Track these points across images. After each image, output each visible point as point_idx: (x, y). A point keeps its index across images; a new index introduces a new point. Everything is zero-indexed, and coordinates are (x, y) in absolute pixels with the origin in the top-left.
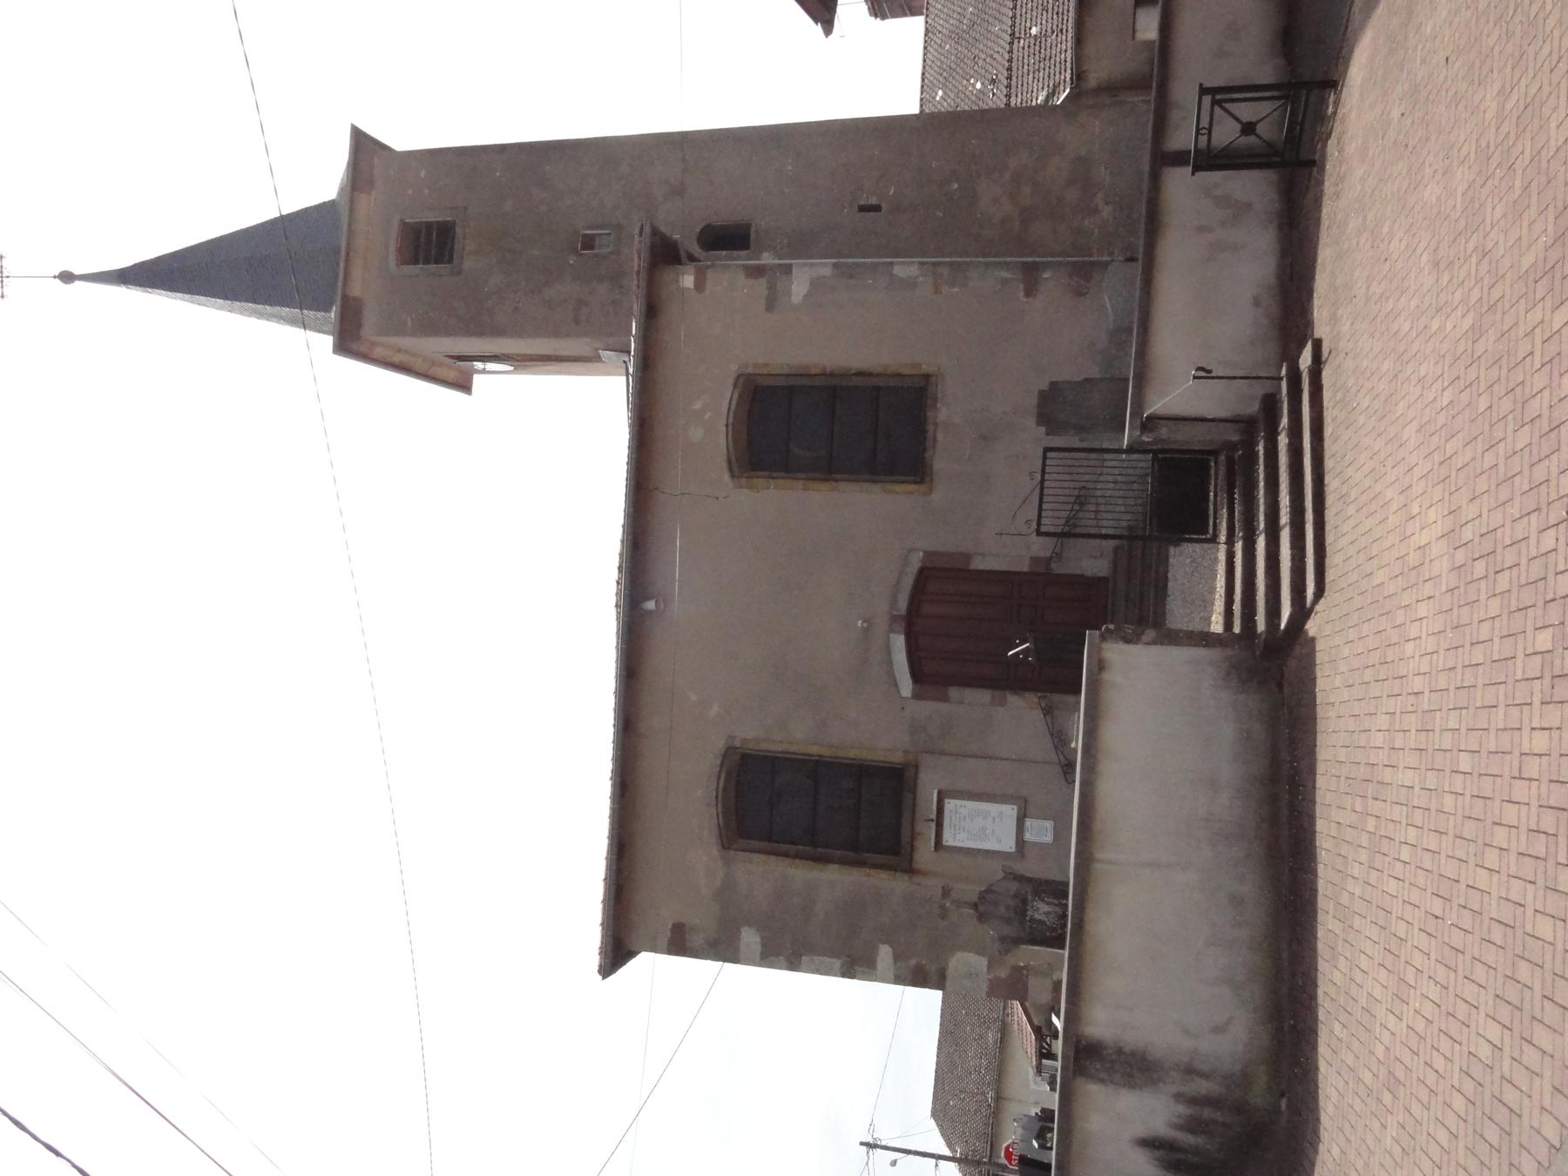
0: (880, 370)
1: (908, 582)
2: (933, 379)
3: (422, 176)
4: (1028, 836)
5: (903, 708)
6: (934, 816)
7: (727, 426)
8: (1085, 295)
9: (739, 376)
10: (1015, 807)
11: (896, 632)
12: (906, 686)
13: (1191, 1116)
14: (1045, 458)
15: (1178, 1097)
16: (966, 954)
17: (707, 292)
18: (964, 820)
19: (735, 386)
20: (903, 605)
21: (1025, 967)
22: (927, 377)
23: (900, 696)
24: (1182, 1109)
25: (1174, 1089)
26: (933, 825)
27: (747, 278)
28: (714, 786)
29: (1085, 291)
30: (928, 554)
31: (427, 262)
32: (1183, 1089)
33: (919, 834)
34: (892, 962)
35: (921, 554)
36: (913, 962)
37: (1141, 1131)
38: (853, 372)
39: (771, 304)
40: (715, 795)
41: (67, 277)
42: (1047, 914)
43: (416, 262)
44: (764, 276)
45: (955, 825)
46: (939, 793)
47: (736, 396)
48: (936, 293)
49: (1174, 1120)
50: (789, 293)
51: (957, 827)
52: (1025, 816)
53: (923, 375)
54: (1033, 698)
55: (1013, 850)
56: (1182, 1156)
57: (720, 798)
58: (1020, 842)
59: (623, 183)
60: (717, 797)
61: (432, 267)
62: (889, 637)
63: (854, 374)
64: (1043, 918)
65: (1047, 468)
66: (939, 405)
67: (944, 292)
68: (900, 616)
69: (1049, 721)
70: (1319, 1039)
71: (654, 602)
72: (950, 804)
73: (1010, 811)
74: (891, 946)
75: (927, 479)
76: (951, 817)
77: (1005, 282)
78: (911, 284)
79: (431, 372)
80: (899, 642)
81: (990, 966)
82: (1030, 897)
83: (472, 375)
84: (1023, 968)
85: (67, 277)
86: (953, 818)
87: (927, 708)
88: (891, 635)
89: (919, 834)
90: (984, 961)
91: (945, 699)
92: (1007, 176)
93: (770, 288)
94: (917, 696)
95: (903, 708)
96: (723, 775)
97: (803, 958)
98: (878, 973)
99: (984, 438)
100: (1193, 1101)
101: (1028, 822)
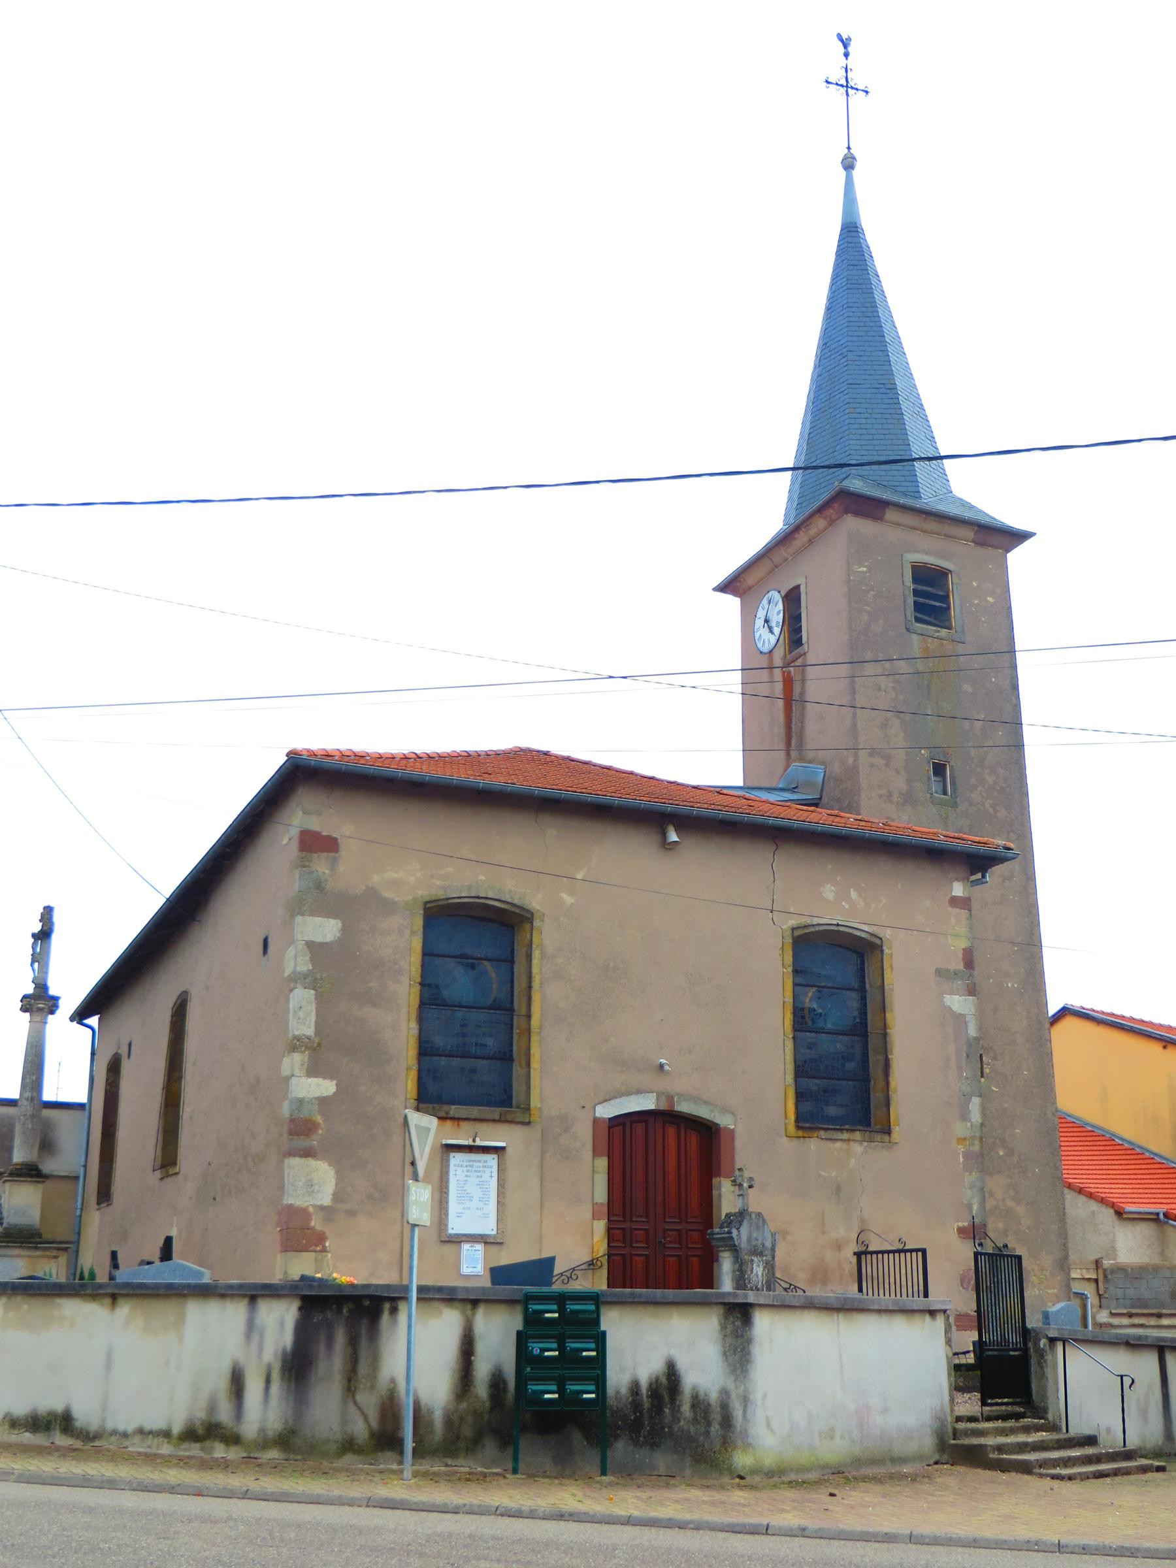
0: (893, 1084)
1: (704, 1112)
2: (886, 1138)
3: (988, 599)
4: (466, 1247)
5: (583, 1107)
6: (479, 1142)
7: (838, 925)
8: (962, 1284)
9: (881, 939)
10: (494, 1232)
11: (658, 1099)
12: (607, 1111)
13: (709, 1404)
14: (917, 1250)
15: (725, 1392)
16: (333, 1182)
17: (950, 909)
18: (478, 1176)
19: (872, 935)
20: (684, 1107)
21: (324, 1250)
22: (889, 1132)
23: (596, 1105)
24: (714, 1396)
25: (731, 1387)
26: (469, 1142)
27: (963, 949)
28: (490, 895)
29: (965, 1286)
30: (732, 1132)
31: (916, 593)
32: (733, 1395)
33: (458, 1125)
34: (316, 1096)
35: (732, 1127)
36: (319, 1119)
37: (682, 1364)
38: (890, 1057)
39: (940, 973)
40: (481, 895)
41: (849, 164)
42: (757, 1275)
43: (915, 580)
44: (965, 968)
45: (471, 1166)
46: (503, 1148)
47: (863, 935)
48: (958, 1139)
49: (702, 1393)
50: (952, 993)
51: (470, 1169)
52: (486, 1243)
53: (890, 1129)
54: (602, 1248)
55: (450, 1231)
56: (667, 1400)
57: (479, 901)
58: (458, 1240)
59: (991, 810)
60: (478, 897)
61: (911, 600)
62: (652, 1092)
63: (887, 1057)
64: (754, 1272)
65: (875, 1255)
66: (865, 1144)
67: (960, 1147)
68: (672, 1104)
69: (583, 1267)
70: (676, 1518)
71: (677, 839)
72: (492, 1160)
73: (489, 1227)
74: (334, 1093)
75: (800, 1133)
76: (480, 1161)
77: (970, 1207)
78: (964, 1116)
79: (766, 561)
80: (647, 1103)
81: (322, 1208)
82: (764, 1258)
83: (739, 597)
84: (324, 1247)
85: (849, 164)
86: (479, 1164)
87: (585, 1133)
88: (655, 1094)
89: (458, 1125)
90: (327, 1201)
91: (596, 1153)
92: (1010, 1203)
93: (956, 974)
94: (596, 1121)
95: (583, 1107)
96: (503, 906)
97: (312, 992)
98: (304, 1079)
99: (838, 1190)
100: (725, 1406)
101: (479, 1247)
